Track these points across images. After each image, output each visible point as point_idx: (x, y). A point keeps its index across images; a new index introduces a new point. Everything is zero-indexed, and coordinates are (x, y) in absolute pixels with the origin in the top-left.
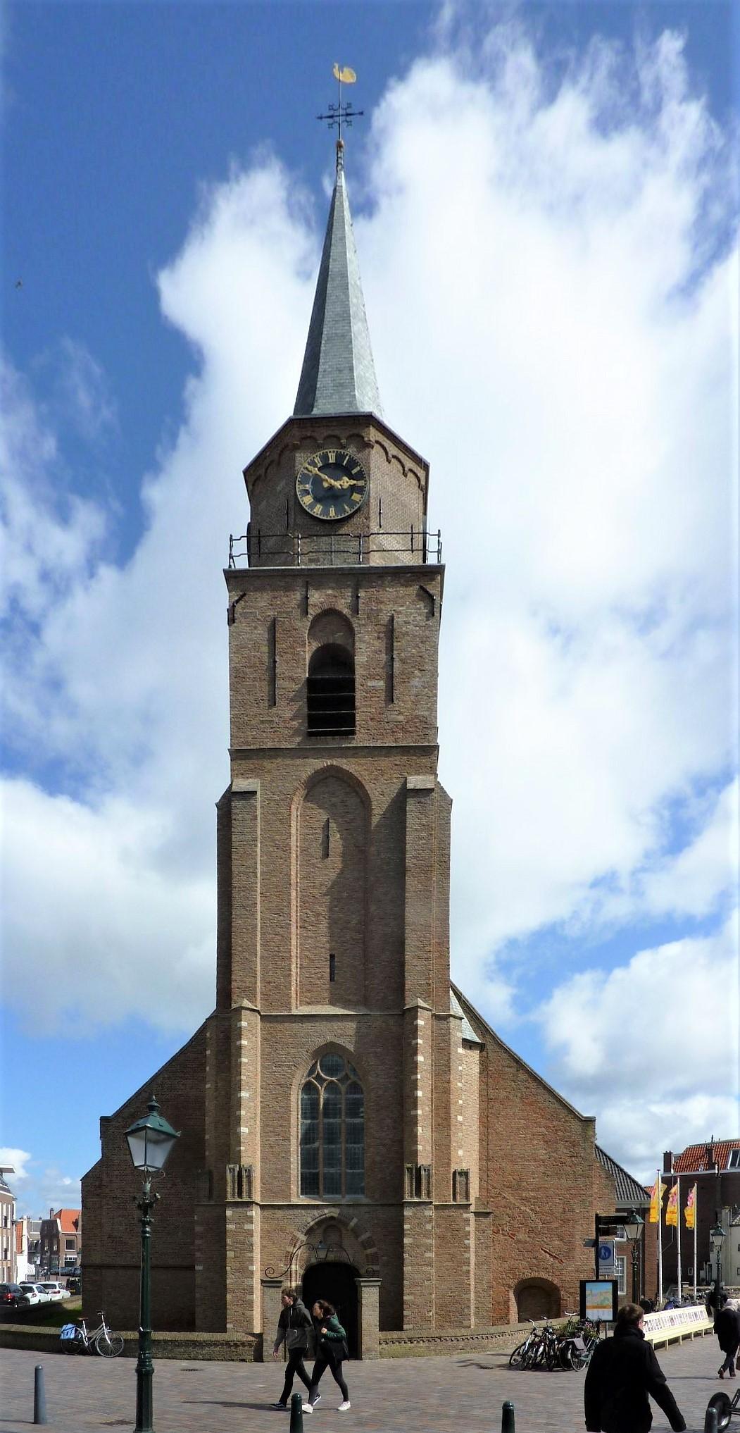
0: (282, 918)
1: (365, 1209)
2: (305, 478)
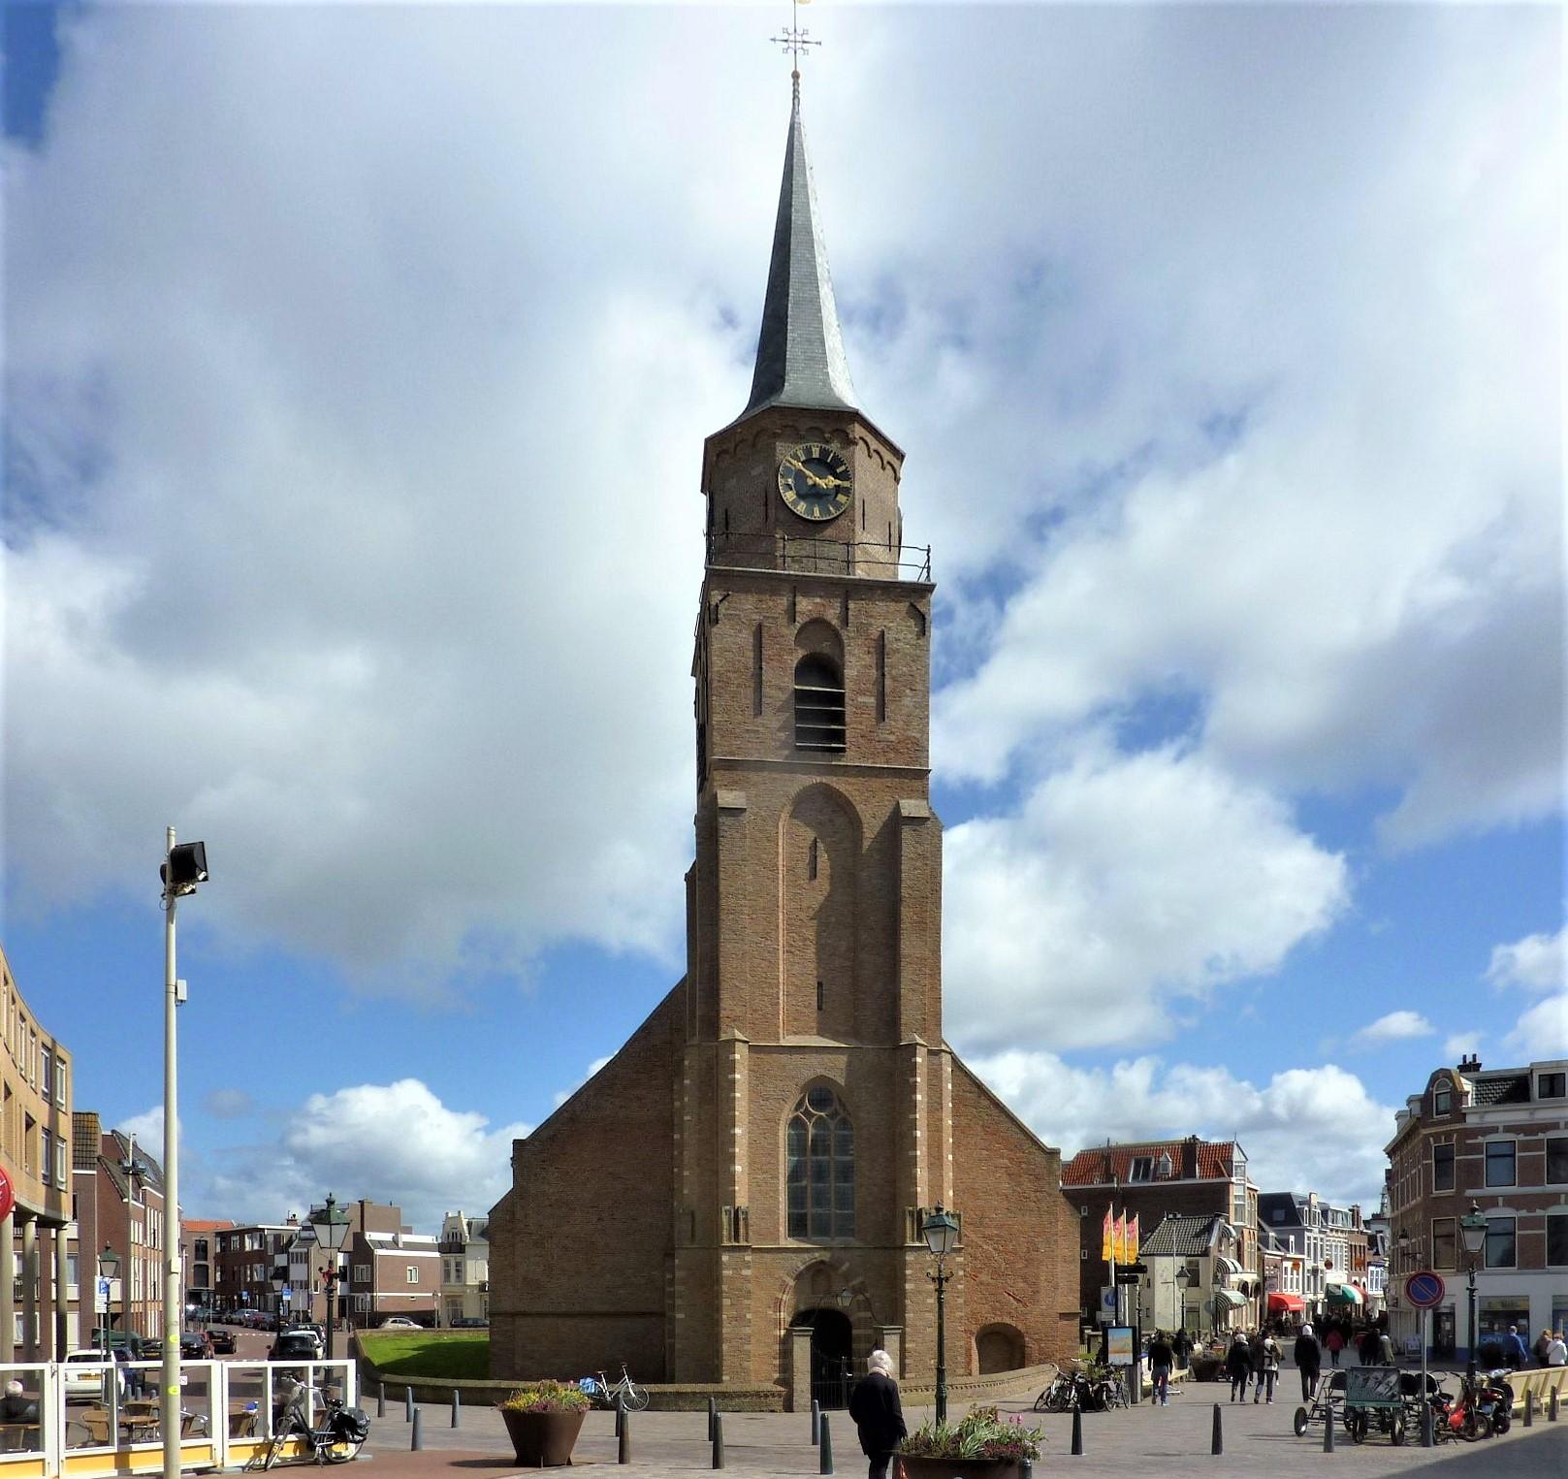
0: (769, 942)
1: (858, 1253)
2: (788, 472)
